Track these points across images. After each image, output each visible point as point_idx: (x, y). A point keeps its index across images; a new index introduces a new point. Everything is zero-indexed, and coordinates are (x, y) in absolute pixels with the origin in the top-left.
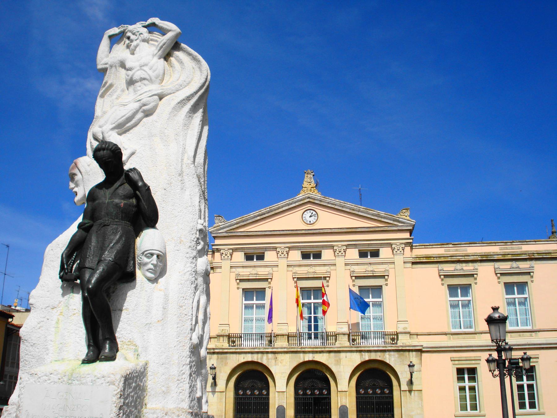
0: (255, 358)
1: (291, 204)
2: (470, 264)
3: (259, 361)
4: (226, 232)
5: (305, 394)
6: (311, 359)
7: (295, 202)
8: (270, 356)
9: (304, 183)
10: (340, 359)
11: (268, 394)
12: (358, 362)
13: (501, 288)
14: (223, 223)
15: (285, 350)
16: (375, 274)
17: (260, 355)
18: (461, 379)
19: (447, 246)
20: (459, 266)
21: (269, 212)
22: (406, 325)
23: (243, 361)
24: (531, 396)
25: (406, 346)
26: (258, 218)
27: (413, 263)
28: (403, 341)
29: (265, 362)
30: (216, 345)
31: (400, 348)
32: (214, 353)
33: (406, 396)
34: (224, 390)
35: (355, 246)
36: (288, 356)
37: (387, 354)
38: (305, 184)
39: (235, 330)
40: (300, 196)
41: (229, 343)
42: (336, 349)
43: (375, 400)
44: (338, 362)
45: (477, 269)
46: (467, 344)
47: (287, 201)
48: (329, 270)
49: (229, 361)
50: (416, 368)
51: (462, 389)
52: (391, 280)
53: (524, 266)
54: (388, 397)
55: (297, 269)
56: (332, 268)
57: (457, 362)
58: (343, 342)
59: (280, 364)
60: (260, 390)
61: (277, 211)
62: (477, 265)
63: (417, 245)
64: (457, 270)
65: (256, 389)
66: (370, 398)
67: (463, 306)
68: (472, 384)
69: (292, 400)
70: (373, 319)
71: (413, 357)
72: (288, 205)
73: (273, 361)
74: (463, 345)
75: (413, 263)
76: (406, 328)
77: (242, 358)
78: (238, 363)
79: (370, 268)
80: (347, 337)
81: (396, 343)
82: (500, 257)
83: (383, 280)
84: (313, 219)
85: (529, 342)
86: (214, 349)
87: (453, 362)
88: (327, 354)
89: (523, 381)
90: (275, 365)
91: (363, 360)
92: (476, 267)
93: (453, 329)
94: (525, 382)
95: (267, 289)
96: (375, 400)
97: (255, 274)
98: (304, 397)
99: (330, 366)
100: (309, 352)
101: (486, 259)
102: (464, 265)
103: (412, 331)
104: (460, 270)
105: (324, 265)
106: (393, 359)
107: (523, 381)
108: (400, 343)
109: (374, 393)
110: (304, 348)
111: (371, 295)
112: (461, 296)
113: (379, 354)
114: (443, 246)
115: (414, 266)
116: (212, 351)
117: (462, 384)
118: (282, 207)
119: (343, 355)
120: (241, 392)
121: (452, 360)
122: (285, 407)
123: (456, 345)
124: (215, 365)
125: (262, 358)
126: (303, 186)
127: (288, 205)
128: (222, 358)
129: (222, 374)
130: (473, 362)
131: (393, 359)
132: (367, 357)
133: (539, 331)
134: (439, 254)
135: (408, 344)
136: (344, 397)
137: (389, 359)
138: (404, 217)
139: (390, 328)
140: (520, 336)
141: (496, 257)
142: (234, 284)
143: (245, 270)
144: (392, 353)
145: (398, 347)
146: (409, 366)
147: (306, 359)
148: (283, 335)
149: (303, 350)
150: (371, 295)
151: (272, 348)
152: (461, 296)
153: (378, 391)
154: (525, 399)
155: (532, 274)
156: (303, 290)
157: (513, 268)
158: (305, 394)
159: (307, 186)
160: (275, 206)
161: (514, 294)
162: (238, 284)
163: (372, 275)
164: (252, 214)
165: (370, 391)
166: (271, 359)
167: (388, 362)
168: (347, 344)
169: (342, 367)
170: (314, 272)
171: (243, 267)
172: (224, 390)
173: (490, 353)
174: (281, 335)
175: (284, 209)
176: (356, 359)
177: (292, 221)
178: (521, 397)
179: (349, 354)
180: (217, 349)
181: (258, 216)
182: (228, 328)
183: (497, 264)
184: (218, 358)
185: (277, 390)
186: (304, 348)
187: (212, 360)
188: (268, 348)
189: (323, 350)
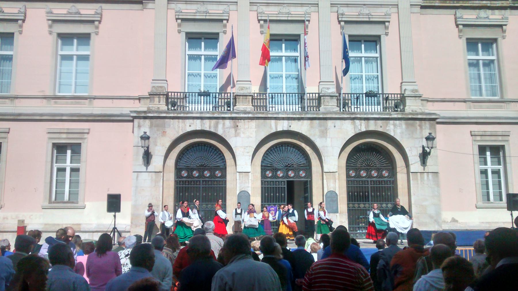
0: (207, 126)
2: (497, 12)
3: (212, 130)
5: (190, 176)
6: (285, 129)
8: (227, 122)
10: (326, 129)
11: (224, 176)
12: (351, 134)
13: (463, 43)
15: (250, 115)
16: (371, 20)
17: (213, 122)
22: (416, 88)
23: (189, 129)
25: (417, 114)
27: (422, 7)
28: (412, 106)
29: (220, 132)
30: (148, 108)
31: (410, 116)
32: (145, 118)
33: (417, 179)
34: (162, 170)
36: (253, 123)
39: (175, 86)
41: (167, 105)
42: (321, 116)
43: (370, 186)
44: (324, 133)
45: (507, 18)
48: (389, 12)
49: (168, 130)
51: (484, 172)
52: (393, 27)
54: (186, 181)
55: (264, 9)
56: (313, 9)
57: (478, 138)
58: (330, 106)
59: (242, 135)
60: (213, 170)
62: (507, 13)
65: (207, 169)
66: (364, 182)
67: (485, 65)
68: (75, 165)
69: (258, 184)
70: (286, 78)
73: (233, 131)
74: (488, 115)
75: (422, 7)
76: (417, 91)
77: (188, 125)
78: (181, 133)
80: (335, 100)
83: (381, 26)
86: (145, 112)
88: (309, 121)
90: (236, 136)
91: (358, 132)
92: (506, 16)
95: (221, 35)
96: (370, 186)
97: (204, 12)
98: (275, 180)
99: (312, 138)
100: (283, 119)
102: (489, 12)
103: (424, 96)
104: (485, 18)
106: (398, 131)
108: (408, 109)
109: (370, 176)
110: (278, 113)
113: (380, 122)
115: (424, 11)
116: (143, 115)
117: (483, 167)
119: (330, 123)
120: (269, 174)
121: (472, 135)
122: (337, 192)
124: (148, 134)
128: (157, 126)
130: (500, 138)
131: (398, 131)
132: (362, 127)
133: (94, 98)
135: (419, 111)
136: (332, 181)
137: (394, 131)
139: (392, 88)
140: (56, 103)
142: (173, 25)
144: (397, 122)
146: (427, 139)
147: (280, 129)
148: (246, 96)
149: (275, 116)
151: (231, 113)
153: (374, 173)
155: (387, 24)
156: (62, 36)
157: (481, 18)
158: (358, 176)
162: (179, 25)
163: (368, 20)
165: (363, 173)
166: (230, 128)
167: (392, 134)
168: (165, 108)
169: (329, 140)
170: (289, 13)
172: (162, 170)
174: (243, 96)
176: (349, 129)
179: (338, 122)
180: (150, 112)
182: (165, 85)
184: (151, 127)
185: (239, 170)
186: (278, 113)
188: (226, 113)
189: (303, 116)
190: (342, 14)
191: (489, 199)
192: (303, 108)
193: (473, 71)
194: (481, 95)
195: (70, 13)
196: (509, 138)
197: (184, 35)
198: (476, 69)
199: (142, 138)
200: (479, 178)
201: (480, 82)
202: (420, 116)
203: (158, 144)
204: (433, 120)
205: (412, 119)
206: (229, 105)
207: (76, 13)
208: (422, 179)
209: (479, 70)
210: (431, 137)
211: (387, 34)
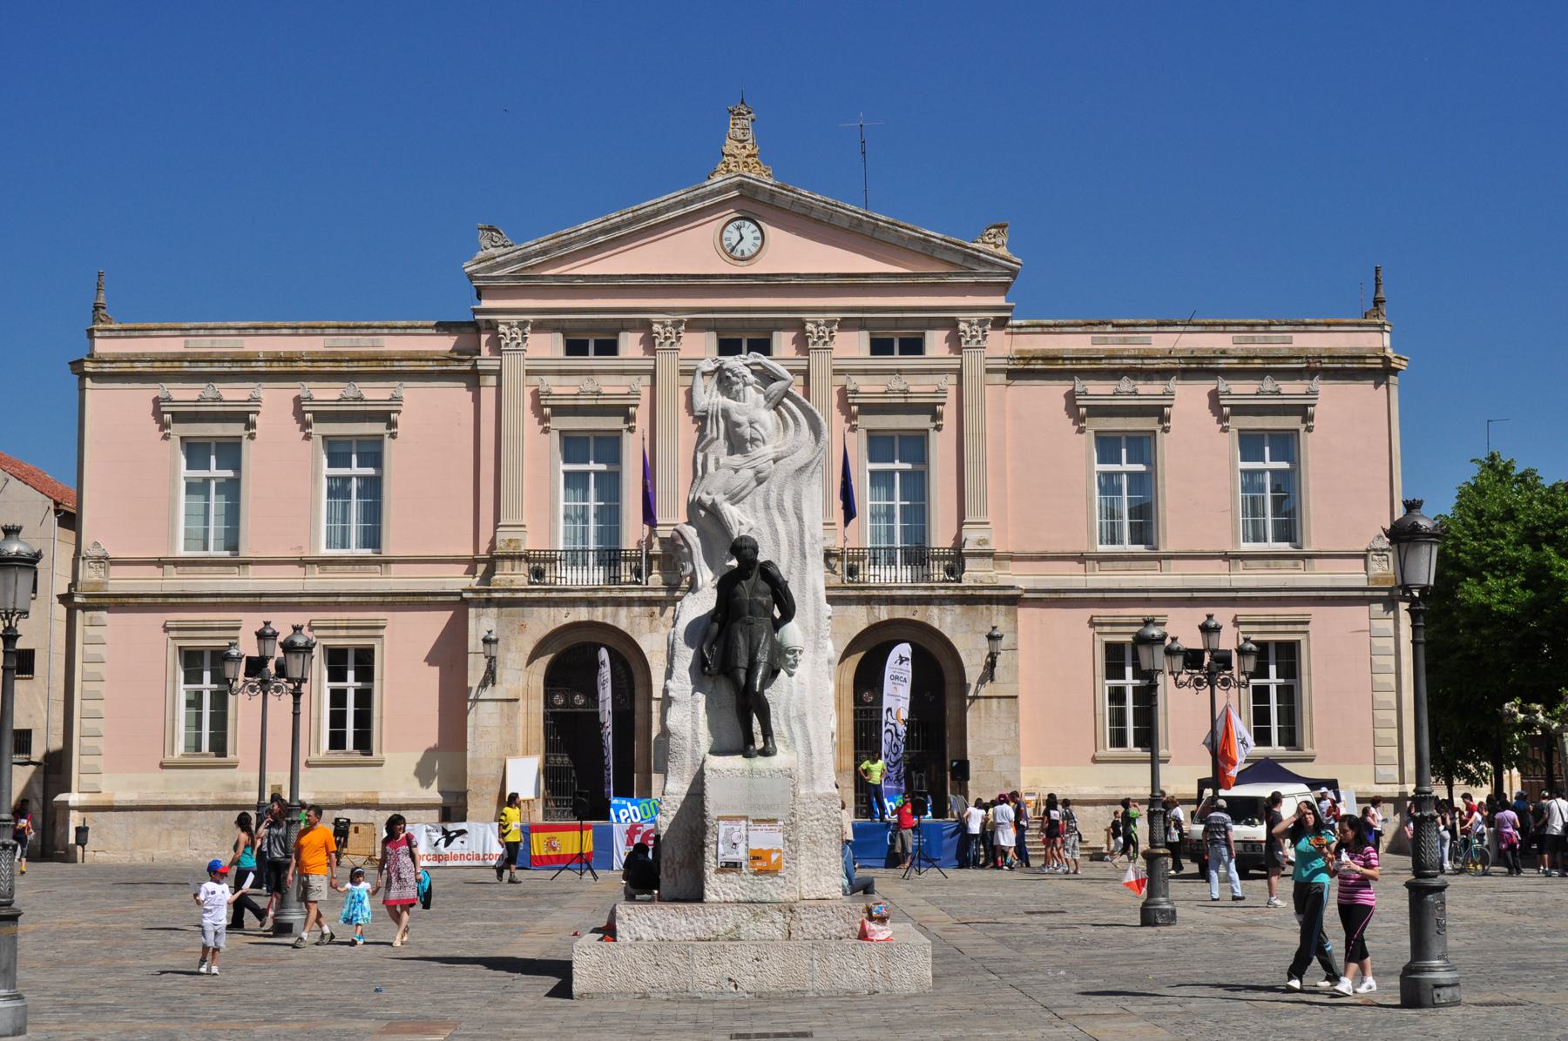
1: (692, 202)
3: (609, 621)
4: (512, 277)
7: (703, 198)
9: (728, 141)
13: (1230, 442)
14: (502, 250)
17: (609, 610)
18: (193, 676)
19: (1100, 328)
20: (1125, 385)
21: (629, 223)
24: (364, 720)
25: (983, 588)
26: (601, 239)
27: (1013, 375)
28: (976, 574)
35: (860, 325)
37: (623, 611)
38: (730, 146)
40: (718, 180)
45: (1315, 393)
46: (214, 590)
47: (681, 194)
49: (527, 621)
50: (1004, 643)
53: (1292, 389)
57: (1107, 629)
61: (652, 222)
62: (1175, 385)
63: (1024, 322)
64: (1121, 393)
71: (998, 617)
72: (685, 203)
73: (646, 622)
76: (985, 542)
79: (896, 383)
81: (960, 581)
82: (1234, 364)
84: (748, 246)
85: (1290, 585)
87: (174, 634)
89: (1123, 677)
92: (1171, 388)
93: (1246, 540)
94: (351, 683)
97: (593, 393)
101: (284, 370)
105: (930, 372)
106: (631, 620)
107: (1123, 677)
108: (968, 579)
111: (213, 459)
112: (1129, 462)
114: (1089, 329)
118: (668, 209)
120: (559, 700)
123: (1328, 584)
125: (615, 616)
126: (726, 150)
127: (685, 203)
129: (510, 656)
132: (883, 613)
134: (1077, 350)
135: (988, 582)
138: (992, 248)
141: (1223, 364)
143: (565, 380)
145: (963, 588)
146: (991, 637)
150: (213, 459)
151: (644, 590)
152: (1129, 462)
154: (1269, 723)
159: (736, 152)
160: (648, 205)
161: (1120, 462)
164: (584, 227)
167: (936, 625)
171: (560, 373)
173: (1210, 610)
175: (672, 215)
177: (692, 250)
178: (337, 719)
181: (604, 231)
183: (1223, 385)
184: (499, 616)
187: (484, 620)
190: (855, 392)
191: (198, 748)
192: (614, 579)
193: (199, 501)
194: (206, 548)
195: (346, 399)
196: (240, 633)
197: (555, 436)
198: (202, 497)
199: (486, 641)
200: (1105, 706)
201: (206, 522)
202: (986, 592)
203: (513, 648)
204: (1012, 600)
205: (970, 600)
206: (639, 575)
207: (214, 400)
208: (988, 709)
209: (207, 499)
210: (269, 631)
211: (938, 428)
